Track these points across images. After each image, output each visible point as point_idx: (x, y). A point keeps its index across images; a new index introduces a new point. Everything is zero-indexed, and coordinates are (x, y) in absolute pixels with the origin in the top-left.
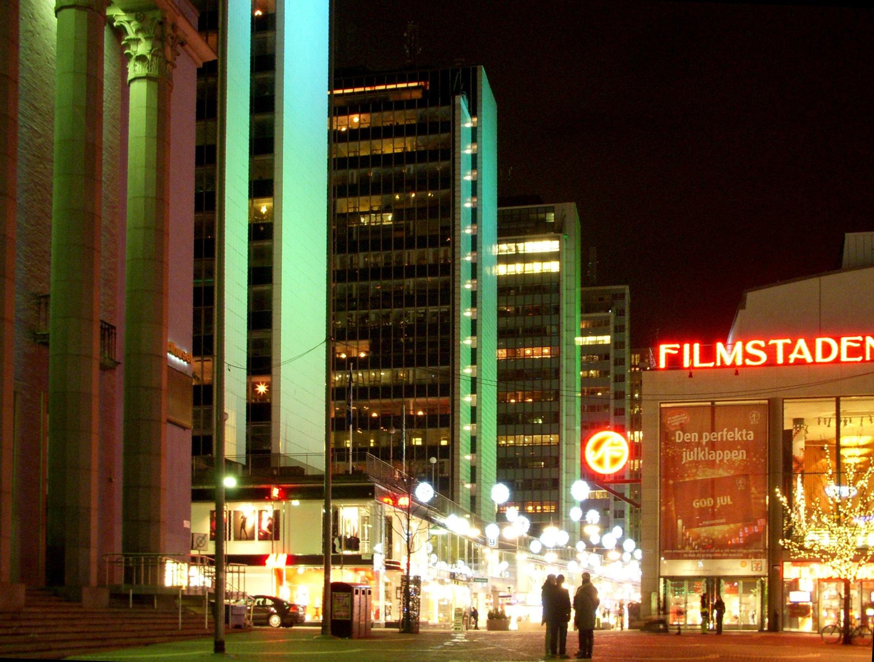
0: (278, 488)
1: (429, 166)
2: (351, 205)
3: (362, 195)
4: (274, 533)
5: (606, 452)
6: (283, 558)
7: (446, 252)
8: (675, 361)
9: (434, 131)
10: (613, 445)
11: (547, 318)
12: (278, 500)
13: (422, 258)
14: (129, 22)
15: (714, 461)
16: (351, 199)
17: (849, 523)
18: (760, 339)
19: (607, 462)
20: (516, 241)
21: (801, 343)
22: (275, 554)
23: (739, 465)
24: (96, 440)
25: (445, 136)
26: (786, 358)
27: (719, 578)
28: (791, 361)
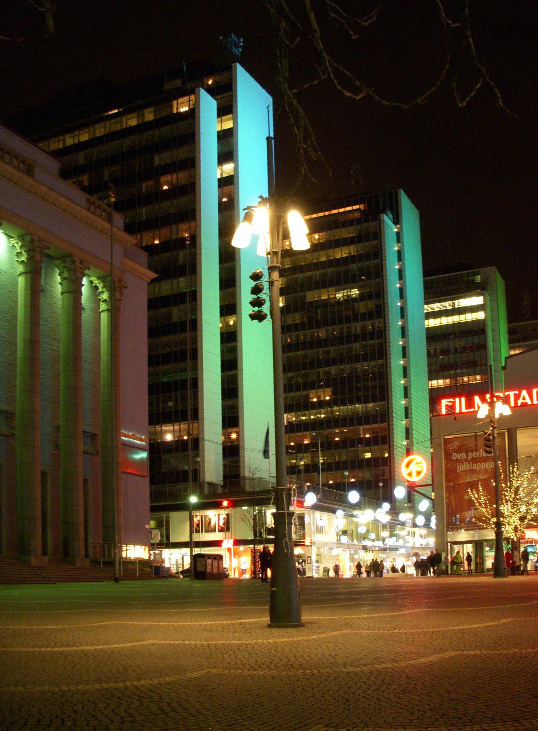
0: (227, 500)
1: (366, 263)
3: (323, 288)
4: (226, 527)
5: (413, 468)
6: (231, 542)
8: (451, 408)
9: (368, 239)
10: (417, 463)
11: (477, 353)
12: (227, 508)
13: (364, 328)
14: (99, 283)
16: (315, 291)
18: (500, 392)
19: (414, 474)
20: (452, 299)
21: (524, 393)
22: (227, 540)
25: (375, 242)
26: (516, 403)
28: (519, 404)
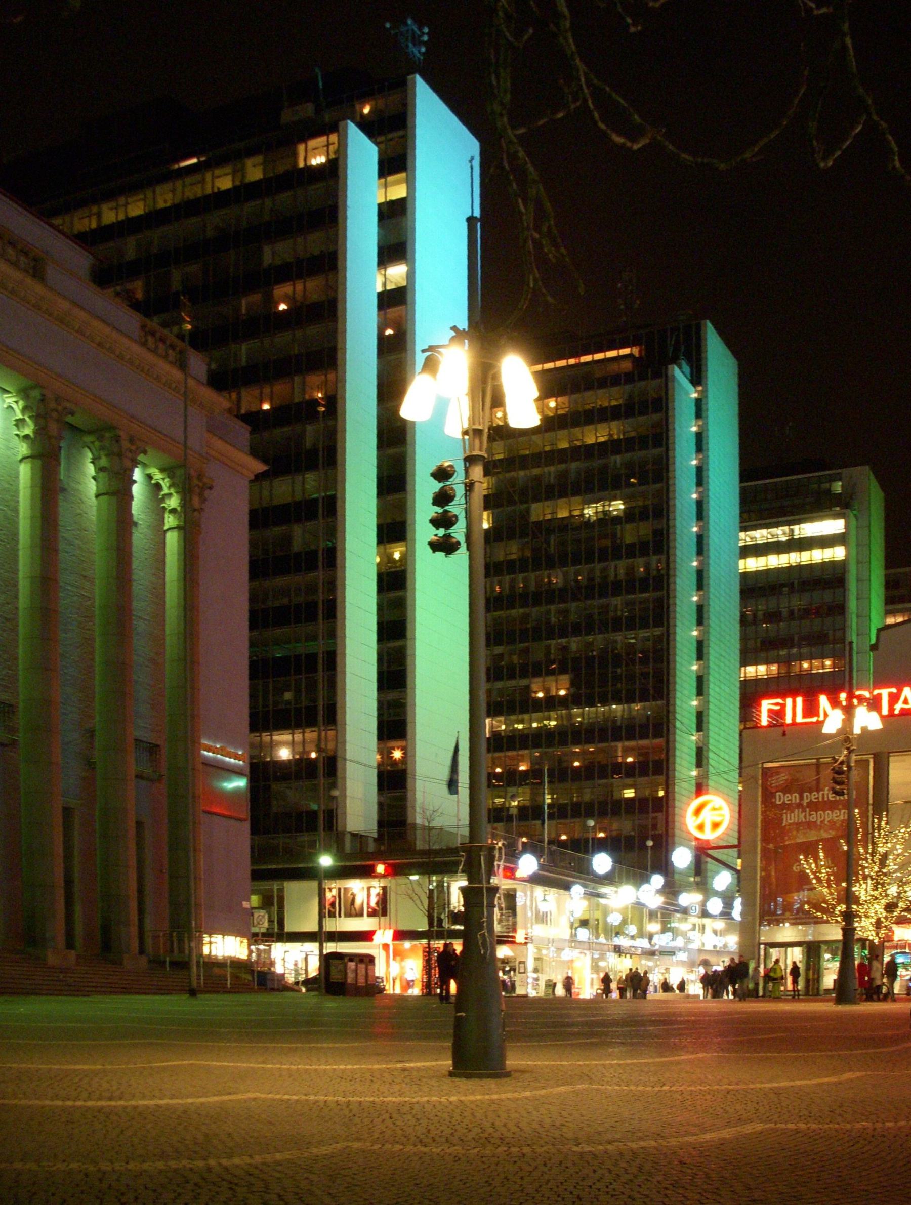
0: (384, 864)
1: (638, 455)
2: (548, 511)
3: (560, 497)
4: (382, 909)
5: (707, 816)
6: (390, 933)
7: (659, 561)
8: (777, 715)
10: (714, 809)
13: (631, 571)
14: (163, 479)
15: (815, 822)
17: (883, 885)
19: (708, 827)
20: (789, 523)
22: (382, 930)
23: (842, 825)
24: (132, 846)
25: (656, 417)
26: (891, 709)
27: (819, 943)
28: (897, 712)
